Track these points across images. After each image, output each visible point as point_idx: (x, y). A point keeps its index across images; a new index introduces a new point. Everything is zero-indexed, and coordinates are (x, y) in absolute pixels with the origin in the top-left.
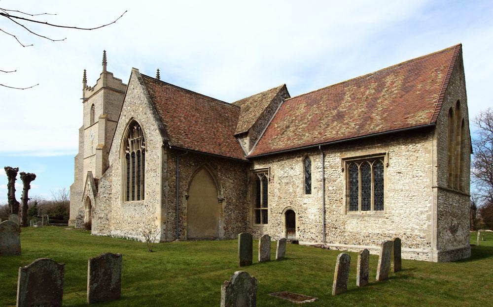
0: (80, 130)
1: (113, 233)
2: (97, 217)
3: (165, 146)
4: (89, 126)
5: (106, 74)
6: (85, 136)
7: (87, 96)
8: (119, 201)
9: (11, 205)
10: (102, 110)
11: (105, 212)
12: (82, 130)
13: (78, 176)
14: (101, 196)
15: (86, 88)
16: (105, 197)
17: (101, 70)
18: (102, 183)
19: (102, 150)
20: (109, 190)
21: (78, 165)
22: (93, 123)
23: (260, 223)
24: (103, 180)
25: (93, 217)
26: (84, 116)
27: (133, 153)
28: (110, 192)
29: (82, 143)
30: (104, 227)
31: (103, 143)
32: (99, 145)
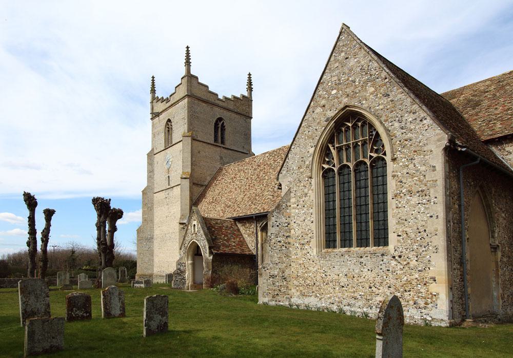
1: (296, 300)
2: (266, 274)
3: (450, 152)
4: (163, 149)
5: (190, 78)
6: (156, 163)
8: (313, 250)
9: (102, 254)
10: (186, 126)
11: (280, 266)
12: (151, 155)
13: (146, 216)
14: (273, 241)
15: (155, 99)
16: (279, 242)
17: (183, 72)
18: (273, 219)
19: (188, 180)
20: (286, 231)
22: (169, 144)
24: (275, 213)
25: (261, 274)
26: (154, 135)
27: (343, 167)
28: (288, 234)
31: (189, 170)
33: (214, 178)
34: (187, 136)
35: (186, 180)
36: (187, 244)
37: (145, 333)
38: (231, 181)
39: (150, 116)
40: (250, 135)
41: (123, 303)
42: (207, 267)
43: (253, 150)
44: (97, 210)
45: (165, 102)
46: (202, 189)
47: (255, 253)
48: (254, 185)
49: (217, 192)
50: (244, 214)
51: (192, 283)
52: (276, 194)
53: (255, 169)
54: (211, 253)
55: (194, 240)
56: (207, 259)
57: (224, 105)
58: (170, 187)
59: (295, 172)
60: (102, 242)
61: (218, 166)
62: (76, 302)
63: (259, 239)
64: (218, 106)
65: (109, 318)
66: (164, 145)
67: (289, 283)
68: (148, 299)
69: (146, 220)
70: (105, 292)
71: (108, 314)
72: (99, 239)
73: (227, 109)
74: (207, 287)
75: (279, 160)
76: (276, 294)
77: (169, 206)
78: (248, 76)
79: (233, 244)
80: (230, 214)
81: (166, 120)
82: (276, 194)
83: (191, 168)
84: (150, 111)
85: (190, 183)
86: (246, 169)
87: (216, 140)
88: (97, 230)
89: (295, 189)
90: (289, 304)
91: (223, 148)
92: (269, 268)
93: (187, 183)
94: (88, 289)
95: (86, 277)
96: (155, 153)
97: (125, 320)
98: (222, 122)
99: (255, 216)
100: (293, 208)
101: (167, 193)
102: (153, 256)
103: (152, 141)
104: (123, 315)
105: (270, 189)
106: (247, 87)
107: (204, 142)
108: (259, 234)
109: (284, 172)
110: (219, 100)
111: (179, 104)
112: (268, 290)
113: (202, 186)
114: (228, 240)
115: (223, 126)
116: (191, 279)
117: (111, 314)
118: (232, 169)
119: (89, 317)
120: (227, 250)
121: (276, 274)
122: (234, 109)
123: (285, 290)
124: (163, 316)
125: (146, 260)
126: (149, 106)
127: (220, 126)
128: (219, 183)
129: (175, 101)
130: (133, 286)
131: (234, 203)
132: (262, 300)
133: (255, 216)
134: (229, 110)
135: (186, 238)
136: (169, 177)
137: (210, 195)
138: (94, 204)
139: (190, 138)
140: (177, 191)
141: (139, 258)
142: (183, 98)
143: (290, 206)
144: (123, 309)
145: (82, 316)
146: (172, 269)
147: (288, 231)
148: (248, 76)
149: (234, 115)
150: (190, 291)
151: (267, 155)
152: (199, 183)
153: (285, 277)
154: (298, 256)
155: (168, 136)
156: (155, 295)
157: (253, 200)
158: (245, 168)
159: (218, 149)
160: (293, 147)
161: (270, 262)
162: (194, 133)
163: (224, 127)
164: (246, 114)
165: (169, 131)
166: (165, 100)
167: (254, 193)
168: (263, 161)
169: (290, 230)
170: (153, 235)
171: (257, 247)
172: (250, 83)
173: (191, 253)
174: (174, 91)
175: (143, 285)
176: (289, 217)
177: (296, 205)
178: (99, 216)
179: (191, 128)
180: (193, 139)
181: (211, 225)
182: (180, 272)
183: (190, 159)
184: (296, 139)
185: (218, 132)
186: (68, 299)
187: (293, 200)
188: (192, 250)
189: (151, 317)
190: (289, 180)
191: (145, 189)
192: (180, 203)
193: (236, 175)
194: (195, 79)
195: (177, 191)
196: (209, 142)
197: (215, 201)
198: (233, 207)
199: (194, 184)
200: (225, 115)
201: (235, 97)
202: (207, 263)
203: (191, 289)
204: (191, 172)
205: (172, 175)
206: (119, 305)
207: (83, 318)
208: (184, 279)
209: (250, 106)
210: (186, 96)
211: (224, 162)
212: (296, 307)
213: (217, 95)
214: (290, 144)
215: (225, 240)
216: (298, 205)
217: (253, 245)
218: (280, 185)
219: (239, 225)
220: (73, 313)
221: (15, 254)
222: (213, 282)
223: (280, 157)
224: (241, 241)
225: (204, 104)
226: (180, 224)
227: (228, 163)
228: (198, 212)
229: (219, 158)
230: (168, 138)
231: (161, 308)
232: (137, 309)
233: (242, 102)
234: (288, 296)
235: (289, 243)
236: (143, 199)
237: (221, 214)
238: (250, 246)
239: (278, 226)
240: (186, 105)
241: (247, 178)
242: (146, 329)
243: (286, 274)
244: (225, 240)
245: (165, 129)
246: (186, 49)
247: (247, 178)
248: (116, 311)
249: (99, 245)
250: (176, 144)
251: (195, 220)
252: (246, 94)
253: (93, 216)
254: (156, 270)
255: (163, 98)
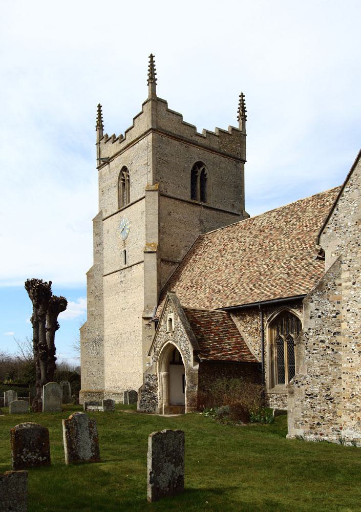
0: (94, 220)
2: (301, 393)
5: (156, 103)
7: (106, 154)
9: (41, 363)
10: (150, 176)
11: (322, 379)
12: (98, 221)
14: (312, 340)
15: (103, 138)
17: (145, 95)
19: (155, 255)
20: (333, 324)
21: (93, 288)
22: (124, 203)
23: (276, 409)
24: (315, 297)
26: (102, 192)
28: (336, 330)
29: (98, 245)
30: (322, 417)
31: (156, 240)
32: (148, 245)
33: (192, 252)
34: (153, 191)
35: (152, 254)
36: (159, 348)
37: (149, 494)
38: (219, 254)
39: (96, 164)
40: (243, 187)
41: (96, 440)
42: (192, 381)
43: (248, 209)
44: (32, 298)
45: (118, 141)
46: (174, 268)
47: (260, 361)
48: (255, 259)
49: (197, 271)
50: (243, 303)
51: (167, 404)
52: (293, 271)
53: (256, 237)
54: (196, 360)
55: (170, 342)
56: (191, 369)
57: (205, 142)
58: (126, 266)
59: (349, 230)
60: (40, 345)
61: (197, 233)
62: (27, 438)
63: (267, 339)
64: (195, 144)
65: (75, 464)
66: (117, 204)
67: (338, 406)
68: (154, 437)
69: (92, 315)
70: (69, 422)
71: (74, 457)
72: (35, 340)
73: (210, 150)
74: (191, 410)
75: (294, 220)
76: (316, 422)
77: (126, 293)
78: (240, 98)
79: (228, 347)
80: (217, 304)
81: (120, 168)
82: (293, 271)
83: (159, 237)
84: (95, 157)
85: (157, 259)
86: (241, 237)
87: (193, 196)
88: (33, 327)
89: (349, 258)
90: (340, 440)
91: (204, 207)
92: (305, 382)
93: (153, 260)
94: (24, 413)
95: (15, 395)
96: (105, 217)
97: (105, 467)
98: (202, 169)
99: (261, 305)
100: (346, 288)
101: (123, 275)
102: (103, 364)
103: (100, 201)
104: (96, 458)
105: (282, 264)
106: (238, 114)
107: (177, 199)
108: (267, 331)
109: (329, 231)
110: (198, 135)
111: (140, 142)
112: (303, 416)
113: (174, 263)
114: (220, 341)
115: (203, 175)
116: (164, 397)
117: (78, 458)
118: (219, 237)
119: (46, 464)
120: (219, 355)
121: (317, 392)
122: (220, 148)
123: (331, 418)
124: (176, 466)
125: (94, 370)
126: (94, 149)
127: (199, 174)
128: (200, 258)
129: (134, 138)
130: (86, 408)
131: (226, 287)
132: (293, 432)
133: (261, 305)
134: (212, 150)
135: (158, 339)
136: (125, 251)
137: (186, 276)
138: (28, 290)
139: (157, 193)
140: (138, 271)
141: (84, 367)
142: (146, 133)
143: (340, 285)
144: (96, 449)
145: (37, 460)
146: (136, 383)
147: (337, 324)
148: (240, 98)
149: (219, 158)
150: (163, 415)
151: (273, 214)
152: (170, 259)
153: (332, 396)
154: (353, 364)
155: (123, 191)
156: (165, 431)
157: (255, 282)
158: (240, 235)
159: (197, 209)
160: (346, 190)
161: (306, 373)
162: (162, 185)
163: (205, 175)
164: (236, 156)
165: (124, 184)
166: (118, 139)
167: (257, 271)
168: (267, 223)
169: (340, 322)
170: (103, 336)
171: (264, 351)
172: (242, 109)
173: (165, 360)
174: (131, 124)
175: (101, 408)
176: (338, 303)
177: (351, 283)
178: (36, 307)
179: (158, 178)
180: (161, 195)
181: (195, 318)
182: (149, 389)
183: (157, 224)
184: (353, 175)
185: (196, 184)
186: (14, 434)
187: (345, 275)
188: (166, 355)
189: (159, 468)
190: (339, 243)
191: (91, 270)
192: (143, 289)
193: (225, 245)
194: (162, 104)
195: (138, 271)
196: (183, 198)
197: (195, 285)
198: (224, 293)
199: (162, 260)
200: (207, 157)
201: (220, 131)
202: (191, 375)
203: (165, 413)
204: (159, 244)
205: (130, 248)
206: (90, 442)
207: (37, 465)
208: (154, 398)
209: (243, 144)
210: (149, 131)
211: (206, 228)
212: (351, 444)
213: (194, 128)
214: (342, 184)
215: (216, 341)
216: (354, 284)
217: (258, 348)
218: (322, 252)
219: (235, 319)
220: (22, 457)
221: (67, 366)
222: (201, 403)
223: (295, 216)
224: (238, 343)
225: (176, 142)
226: (145, 318)
227: (211, 229)
228: (176, 301)
229: (198, 222)
230: (123, 195)
231: (174, 451)
232: (111, 446)
233: (231, 138)
234: (336, 426)
235: (338, 344)
236: (88, 284)
237: (207, 304)
238: (252, 349)
239: (320, 317)
240: (151, 144)
241: (244, 250)
242: (153, 488)
243: (333, 392)
244: (216, 341)
245: (119, 183)
246: (149, 59)
247: (244, 250)
248: (86, 453)
249: (36, 348)
250: (135, 203)
251: (171, 312)
252: (237, 125)
253: (27, 308)
254: (108, 386)
255: (114, 136)
